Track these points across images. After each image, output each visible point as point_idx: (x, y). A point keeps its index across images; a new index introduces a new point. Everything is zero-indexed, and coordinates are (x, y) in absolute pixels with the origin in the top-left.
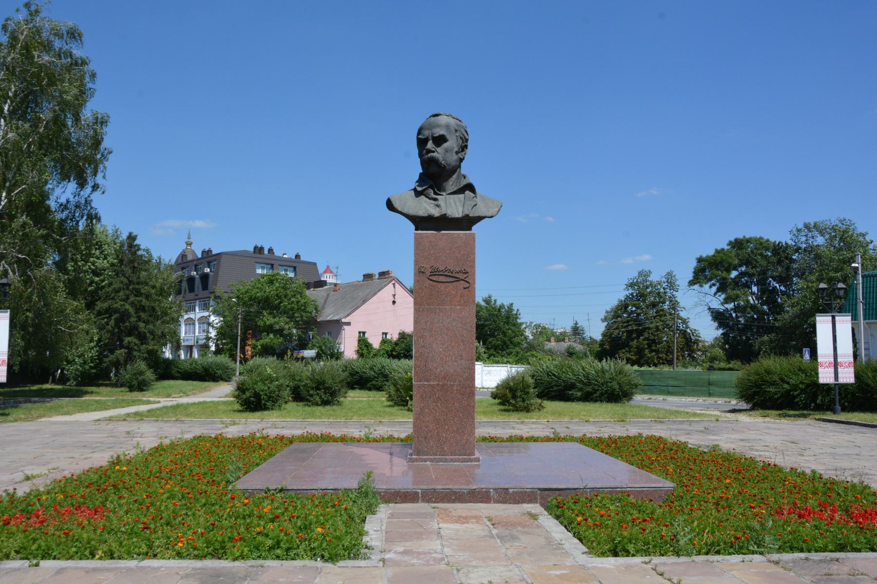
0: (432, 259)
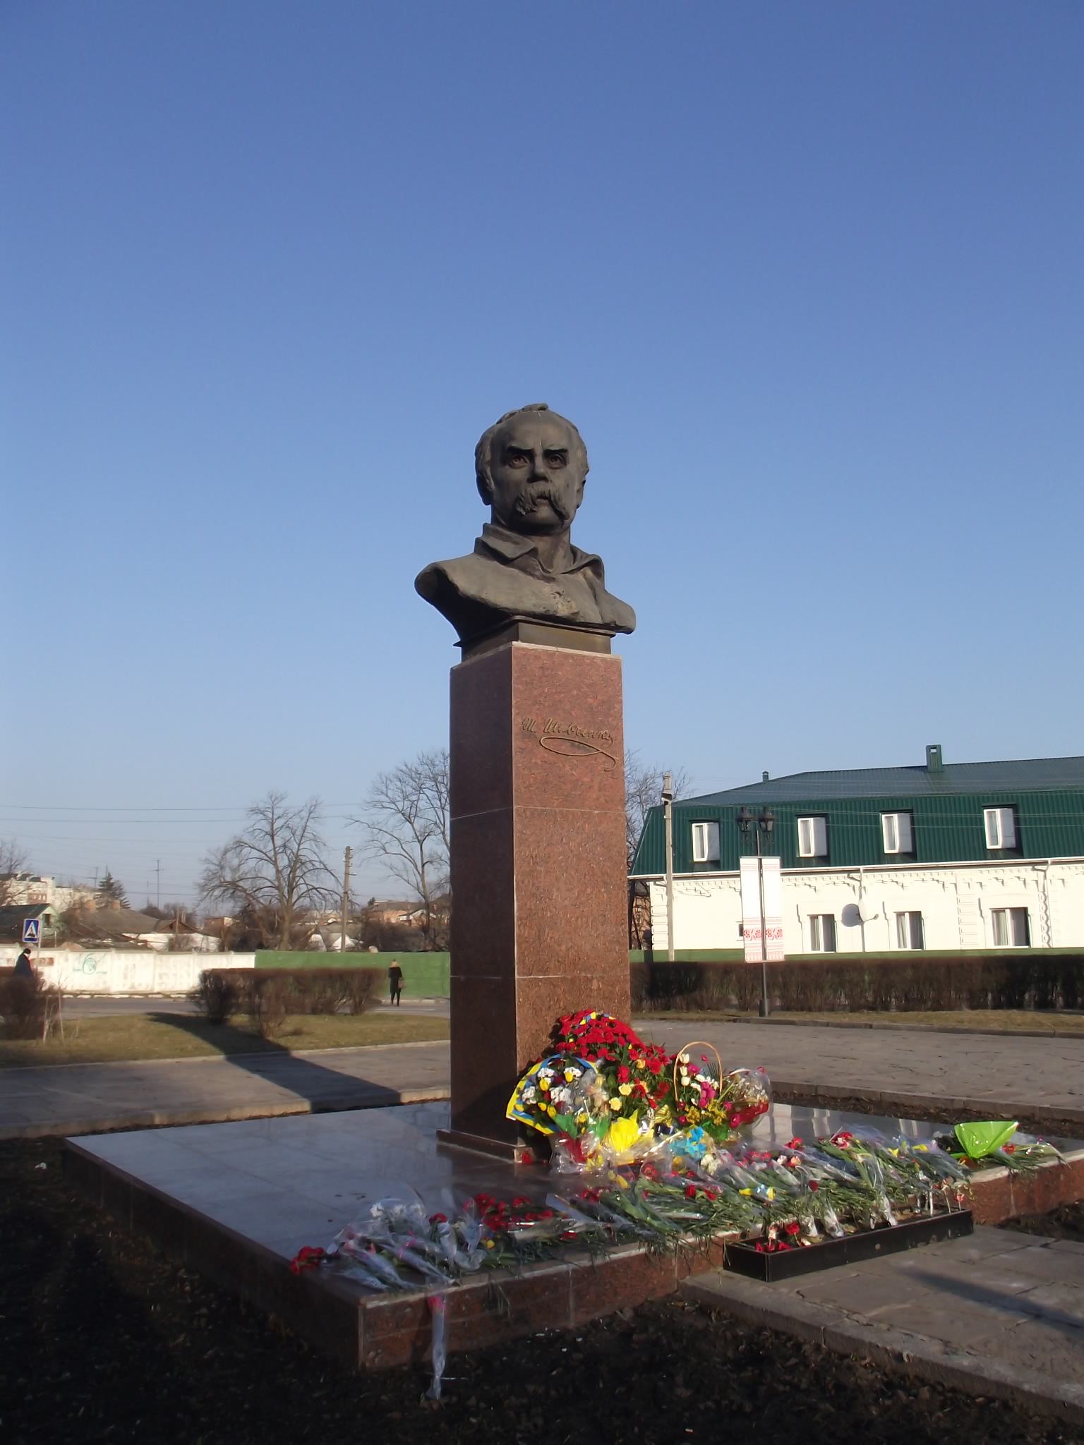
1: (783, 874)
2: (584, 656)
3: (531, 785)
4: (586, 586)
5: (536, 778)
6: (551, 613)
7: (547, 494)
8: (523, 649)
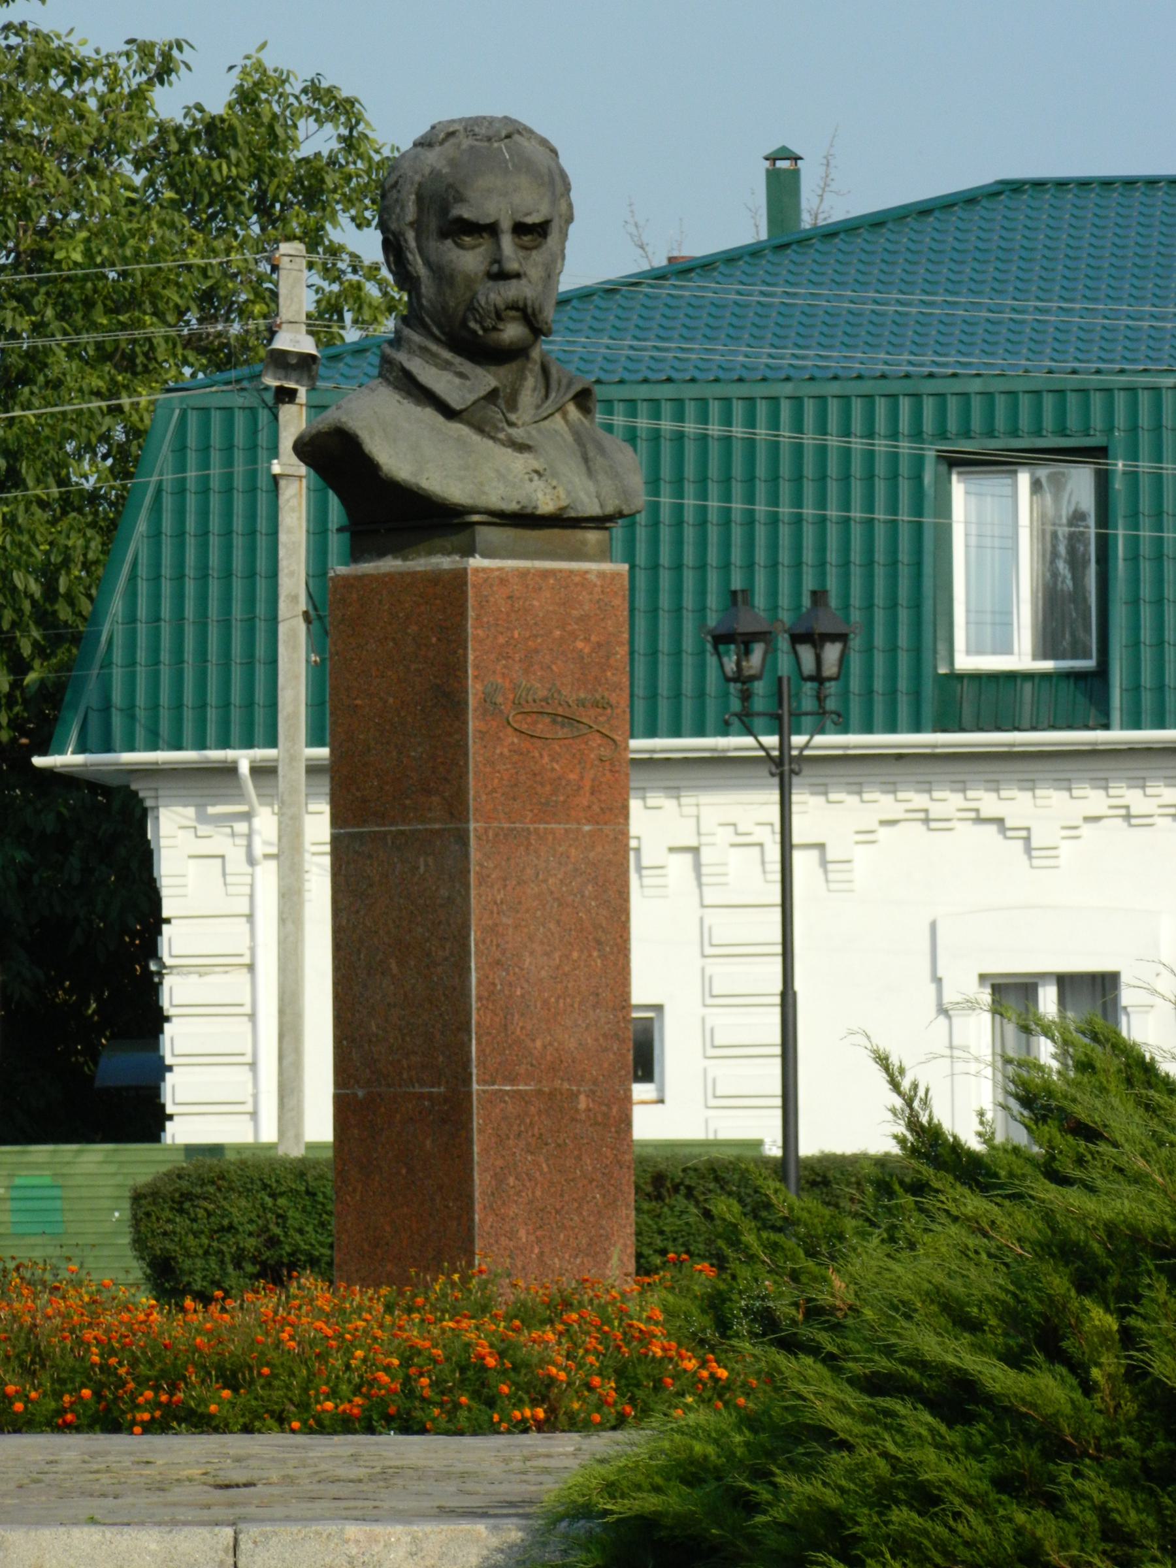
0: (517, 657)
1: (725, 864)
2: (571, 572)
3: (494, 790)
4: (570, 438)
5: (501, 779)
6: (529, 511)
7: (521, 304)
8: (484, 570)
